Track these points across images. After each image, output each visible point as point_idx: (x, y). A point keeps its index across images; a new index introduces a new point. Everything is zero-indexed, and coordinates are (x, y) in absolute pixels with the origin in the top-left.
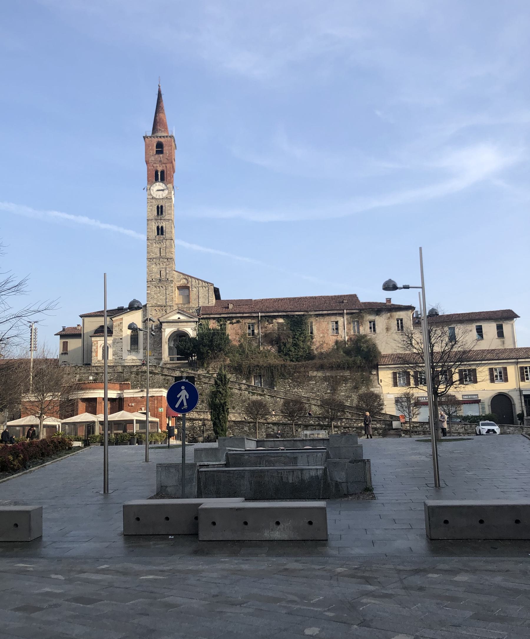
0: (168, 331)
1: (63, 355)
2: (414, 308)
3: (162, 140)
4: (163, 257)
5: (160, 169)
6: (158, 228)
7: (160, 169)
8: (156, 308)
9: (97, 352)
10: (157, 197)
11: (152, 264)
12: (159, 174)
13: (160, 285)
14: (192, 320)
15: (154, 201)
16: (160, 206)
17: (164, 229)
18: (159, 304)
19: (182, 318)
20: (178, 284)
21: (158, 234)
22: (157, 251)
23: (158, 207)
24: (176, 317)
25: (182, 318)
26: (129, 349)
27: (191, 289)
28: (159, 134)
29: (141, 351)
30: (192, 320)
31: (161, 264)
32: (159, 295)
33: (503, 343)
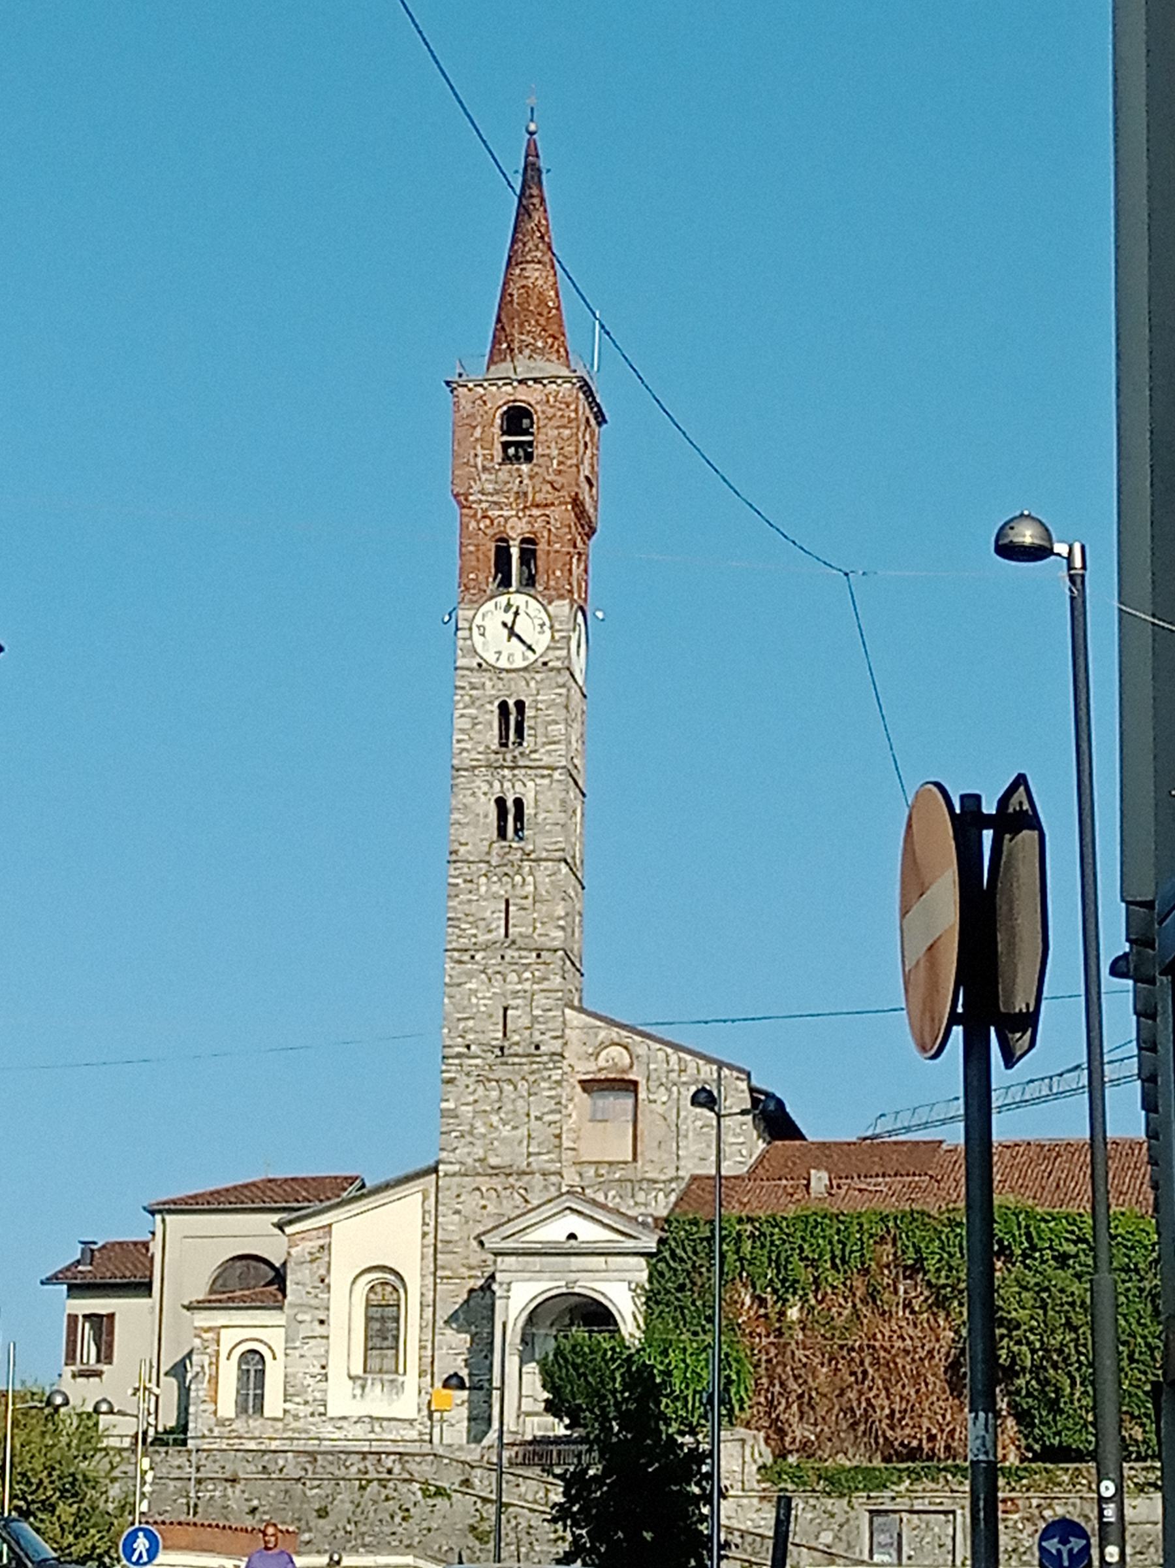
0: (519, 1297)
1: (80, 1380)
2: (109, 1360)
3: (528, 396)
4: (520, 942)
5: (517, 530)
6: (501, 803)
7: (517, 530)
8: (484, 1183)
9: (214, 1380)
10: (503, 663)
11: (470, 975)
12: (515, 552)
13: (500, 1072)
14: (630, 1244)
15: (485, 678)
16: (511, 702)
17: (528, 811)
18: (493, 1161)
19: (589, 1232)
20: (587, 1069)
21: (502, 833)
22: (493, 912)
23: (503, 706)
24: (555, 1231)
25: (589, 1232)
26: (358, 1370)
27: (642, 1095)
28: (524, 366)
29: (411, 1380)
30: (630, 1244)
31: (513, 977)
32: (495, 1119)
33: (498, 659)
